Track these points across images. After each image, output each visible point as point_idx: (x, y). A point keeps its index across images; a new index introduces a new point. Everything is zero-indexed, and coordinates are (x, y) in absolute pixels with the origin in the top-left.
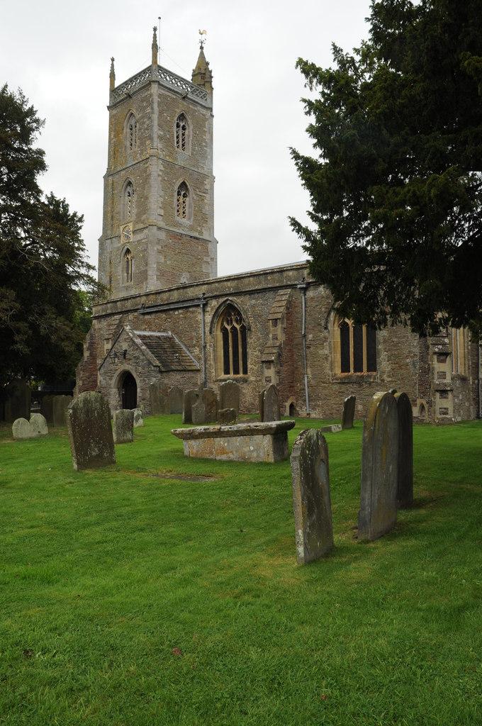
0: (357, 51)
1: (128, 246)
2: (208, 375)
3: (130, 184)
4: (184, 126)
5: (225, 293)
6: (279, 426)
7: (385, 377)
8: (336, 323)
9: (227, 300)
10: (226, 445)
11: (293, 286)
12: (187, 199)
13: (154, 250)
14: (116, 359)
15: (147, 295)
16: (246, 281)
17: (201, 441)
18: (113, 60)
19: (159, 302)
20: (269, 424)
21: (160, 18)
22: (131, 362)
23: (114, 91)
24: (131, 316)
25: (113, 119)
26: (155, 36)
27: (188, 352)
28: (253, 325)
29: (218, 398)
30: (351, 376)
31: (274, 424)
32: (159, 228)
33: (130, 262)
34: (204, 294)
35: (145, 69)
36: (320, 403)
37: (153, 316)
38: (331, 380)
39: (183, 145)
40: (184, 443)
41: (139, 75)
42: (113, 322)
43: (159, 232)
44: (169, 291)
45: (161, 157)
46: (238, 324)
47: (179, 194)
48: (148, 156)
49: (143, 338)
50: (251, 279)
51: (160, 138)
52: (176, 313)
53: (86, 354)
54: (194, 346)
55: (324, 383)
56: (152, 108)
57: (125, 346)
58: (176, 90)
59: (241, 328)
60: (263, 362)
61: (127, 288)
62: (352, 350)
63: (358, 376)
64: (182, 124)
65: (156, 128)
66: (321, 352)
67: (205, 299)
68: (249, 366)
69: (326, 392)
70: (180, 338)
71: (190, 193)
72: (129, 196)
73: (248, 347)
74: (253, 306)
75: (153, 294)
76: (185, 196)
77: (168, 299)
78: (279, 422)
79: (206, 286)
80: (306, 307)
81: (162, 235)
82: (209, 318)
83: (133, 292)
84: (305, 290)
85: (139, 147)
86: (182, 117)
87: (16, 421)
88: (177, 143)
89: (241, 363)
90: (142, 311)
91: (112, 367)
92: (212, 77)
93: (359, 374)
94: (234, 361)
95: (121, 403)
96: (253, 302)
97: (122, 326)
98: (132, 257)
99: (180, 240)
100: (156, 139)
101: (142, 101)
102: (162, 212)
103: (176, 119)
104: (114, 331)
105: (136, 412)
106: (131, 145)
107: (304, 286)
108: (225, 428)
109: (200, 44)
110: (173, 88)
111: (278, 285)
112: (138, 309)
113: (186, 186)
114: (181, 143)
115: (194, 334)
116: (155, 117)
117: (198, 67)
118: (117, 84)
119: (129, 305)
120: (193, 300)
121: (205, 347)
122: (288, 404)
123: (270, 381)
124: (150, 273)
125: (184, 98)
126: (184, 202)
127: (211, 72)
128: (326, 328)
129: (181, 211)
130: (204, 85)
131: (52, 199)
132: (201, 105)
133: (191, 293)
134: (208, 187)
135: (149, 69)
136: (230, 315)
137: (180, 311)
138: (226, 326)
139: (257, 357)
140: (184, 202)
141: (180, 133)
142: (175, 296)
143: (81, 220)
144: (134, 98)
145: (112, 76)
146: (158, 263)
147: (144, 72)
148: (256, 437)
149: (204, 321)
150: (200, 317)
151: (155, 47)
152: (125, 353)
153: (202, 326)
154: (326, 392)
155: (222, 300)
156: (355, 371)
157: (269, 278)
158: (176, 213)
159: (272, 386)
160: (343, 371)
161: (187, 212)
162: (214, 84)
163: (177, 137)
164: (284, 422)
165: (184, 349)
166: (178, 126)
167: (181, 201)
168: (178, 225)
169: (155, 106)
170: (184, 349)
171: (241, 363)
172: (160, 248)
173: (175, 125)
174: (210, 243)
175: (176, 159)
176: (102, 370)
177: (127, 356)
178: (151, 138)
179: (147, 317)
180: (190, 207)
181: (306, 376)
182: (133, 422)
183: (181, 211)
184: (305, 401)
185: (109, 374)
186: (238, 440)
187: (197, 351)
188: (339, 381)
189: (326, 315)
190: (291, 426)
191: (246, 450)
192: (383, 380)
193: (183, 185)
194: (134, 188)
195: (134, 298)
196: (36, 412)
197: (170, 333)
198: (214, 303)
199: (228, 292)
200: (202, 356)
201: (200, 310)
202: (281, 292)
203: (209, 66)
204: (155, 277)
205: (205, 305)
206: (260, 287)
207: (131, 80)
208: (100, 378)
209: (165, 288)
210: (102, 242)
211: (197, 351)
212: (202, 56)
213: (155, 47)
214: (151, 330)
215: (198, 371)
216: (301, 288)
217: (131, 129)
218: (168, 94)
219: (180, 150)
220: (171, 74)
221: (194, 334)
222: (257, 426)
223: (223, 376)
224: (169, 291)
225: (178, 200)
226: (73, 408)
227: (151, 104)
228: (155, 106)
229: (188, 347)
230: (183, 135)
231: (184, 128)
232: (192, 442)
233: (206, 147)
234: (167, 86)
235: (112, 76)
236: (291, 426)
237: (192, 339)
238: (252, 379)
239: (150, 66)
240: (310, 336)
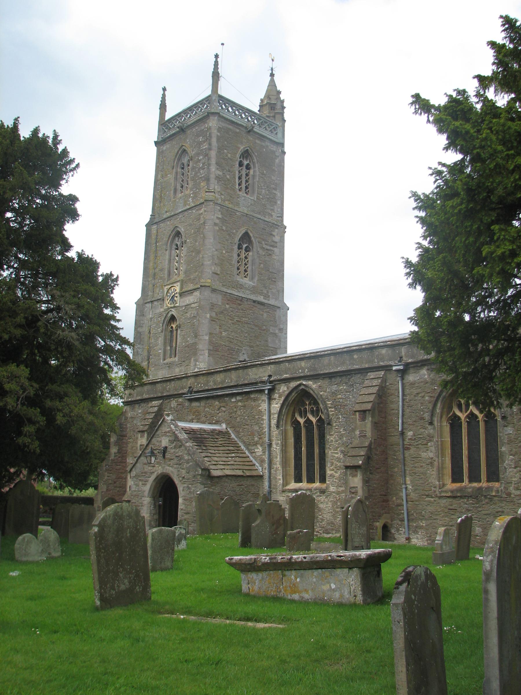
0: (422, 228)
1: (174, 312)
2: (273, 482)
3: (178, 234)
4: (248, 165)
5: (298, 375)
6: (370, 558)
7: (511, 489)
8: (444, 416)
9: (300, 385)
10: (298, 580)
11: (387, 368)
12: (250, 254)
13: (206, 318)
14: (153, 459)
15: (196, 376)
16: (326, 360)
17: (265, 574)
18: (164, 89)
19: (211, 385)
20: (357, 553)
21: (223, 44)
22: (172, 462)
23: (163, 124)
24: (174, 403)
25: (160, 155)
26: (216, 64)
27: (247, 452)
28: (334, 419)
29: (287, 515)
30: (465, 487)
31: (363, 554)
32: (214, 291)
33: (175, 332)
34: (270, 376)
35: (203, 100)
36: (423, 524)
37: (203, 403)
38: (437, 493)
39: (247, 188)
40: (243, 576)
41: (196, 106)
42: (151, 410)
43: (213, 295)
44: (225, 371)
45: (219, 201)
46: (314, 416)
47: (240, 247)
48: (202, 201)
49: (190, 432)
50: (332, 358)
51: (218, 178)
52: (233, 400)
53: (114, 450)
54: (256, 444)
55: (428, 496)
56: (210, 144)
57: (165, 442)
58: (240, 123)
59: (318, 421)
60: (347, 467)
61: (170, 366)
62: (465, 452)
63: (474, 488)
64: (245, 163)
65: (213, 168)
66: (424, 455)
67: (271, 382)
68: (329, 472)
69: (430, 508)
70: (237, 433)
71: (255, 246)
72: (177, 249)
73: (327, 446)
74: (334, 394)
75: (203, 374)
76: (247, 250)
77: (223, 382)
78: (369, 552)
79: (272, 366)
80: (403, 395)
81: (218, 299)
82: (276, 406)
83: (177, 371)
84: (403, 373)
85: (191, 190)
86: (246, 154)
87: (20, 538)
88: (239, 185)
89: (317, 467)
90: (189, 396)
91: (148, 468)
92: (284, 108)
93: (475, 485)
94: (308, 465)
95: (156, 517)
96: (334, 388)
97: (162, 415)
98: (178, 327)
99: (240, 305)
100: (213, 180)
101: (198, 136)
102: (218, 270)
103: (238, 156)
104: (150, 421)
105: (178, 530)
106: (182, 187)
107: (401, 367)
108: (297, 557)
109: (271, 72)
110: (236, 121)
111: (367, 366)
112: (184, 394)
113: (249, 237)
114: (243, 186)
115: (256, 428)
116: (213, 154)
117: (268, 96)
118: (168, 116)
119: (171, 388)
120: (256, 383)
121: (270, 445)
122: (379, 525)
123: (356, 493)
124: (200, 347)
125: (249, 131)
126: (246, 258)
127: (283, 102)
128: (431, 423)
129: (242, 269)
130: (274, 117)
131: (80, 255)
132: (271, 140)
133: (253, 375)
134: (277, 239)
135: (208, 99)
136: (304, 404)
137: (239, 398)
138: (299, 419)
139: (339, 459)
140: (246, 258)
141: (244, 172)
142: (233, 378)
143: (117, 279)
144: (189, 132)
145: (163, 107)
146: (210, 334)
147: (201, 102)
148: (338, 571)
149: (270, 411)
150: (264, 406)
151: (216, 76)
152: (165, 450)
153: (266, 417)
154: (430, 508)
155: (293, 384)
156: (470, 481)
157: (355, 356)
158: (236, 272)
159: (360, 501)
160: (454, 481)
161: (249, 270)
162: (286, 116)
163: (240, 178)
164: (377, 550)
165: (243, 447)
166: (241, 164)
167: (243, 256)
168: (241, 287)
169: (214, 141)
170: (243, 447)
171: (317, 467)
172: (214, 314)
173: (237, 163)
174: (278, 310)
175: (238, 204)
176: (133, 473)
177: (168, 455)
178: (207, 180)
179: (195, 404)
180: (253, 264)
181: (404, 486)
182: (174, 544)
183: (242, 269)
184: (403, 521)
185: (141, 477)
186: (313, 576)
187: (259, 450)
188: (449, 494)
189: (430, 406)
190: (386, 556)
191: (325, 587)
192: (509, 494)
193: (246, 237)
194: (184, 238)
195: (179, 379)
196: (44, 524)
197: (224, 426)
198: (283, 389)
199: (302, 375)
200: (266, 458)
201: (265, 398)
202: (371, 375)
203: (281, 96)
204: (206, 353)
205: (271, 391)
206: (343, 368)
207: (185, 112)
208: (130, 482)
209: (220, 367)
210: (141, 306)
211: (259, 450)
212: (272, 84)
213: (216, 76)
214: (199, 421)
215: (261, 477)
216: (398, 371)
217: (183, 168)
218: (230, 127)
219: (242, 194)
220: (233, 104)
221: (256, 428)
222: (341, 556)
223: (293, 485)
224: (225, 371)
225: (239, 255)
226: (99, 525)
227: (208, 139)
228: (214, 141)
229: (247, 446)
230: (247, 175)
231: (248, 167)
232: (253, 576)
233: (275, 189)
234: (229, 118)
235: (163, 107)
236: (386, 556)
237: (253, 434)
238: (332, 489)
239: (209, 96)
240: (410, 433)
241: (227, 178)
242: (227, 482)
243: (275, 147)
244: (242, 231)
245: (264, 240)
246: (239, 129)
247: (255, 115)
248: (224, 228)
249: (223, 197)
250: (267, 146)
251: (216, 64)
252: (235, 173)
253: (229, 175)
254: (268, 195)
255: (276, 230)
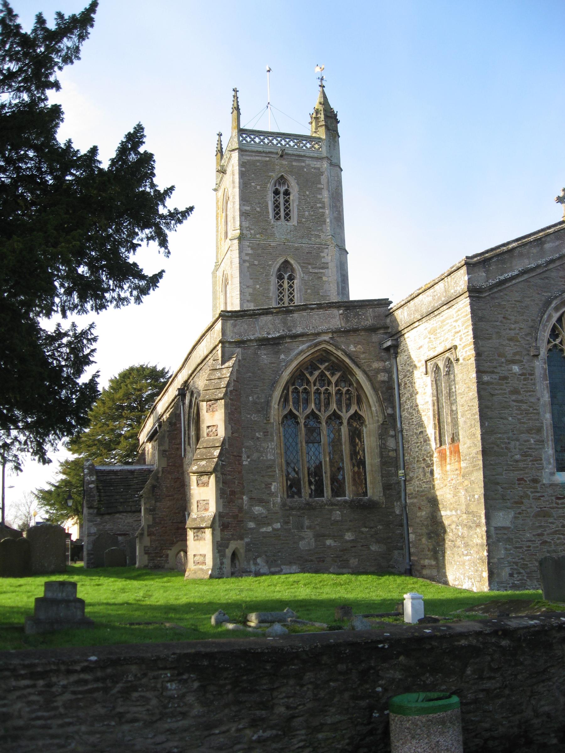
26: (236, 97)
64: (282, 189)
114: (282, 214)
125: (281, 156)
241: (257, 212)
242: (121, 518)
243: (319, 163)
244: (281, 260)
245: (309, 264)
246: (269, 157)
247: (246, 132)
248: (256, 263)
249: (252, 232)
250: (309, 165)
251: (236, 97)
252: (267, 203)
253: (260, 207)
254: (313, 216)
255: (326, 251)
